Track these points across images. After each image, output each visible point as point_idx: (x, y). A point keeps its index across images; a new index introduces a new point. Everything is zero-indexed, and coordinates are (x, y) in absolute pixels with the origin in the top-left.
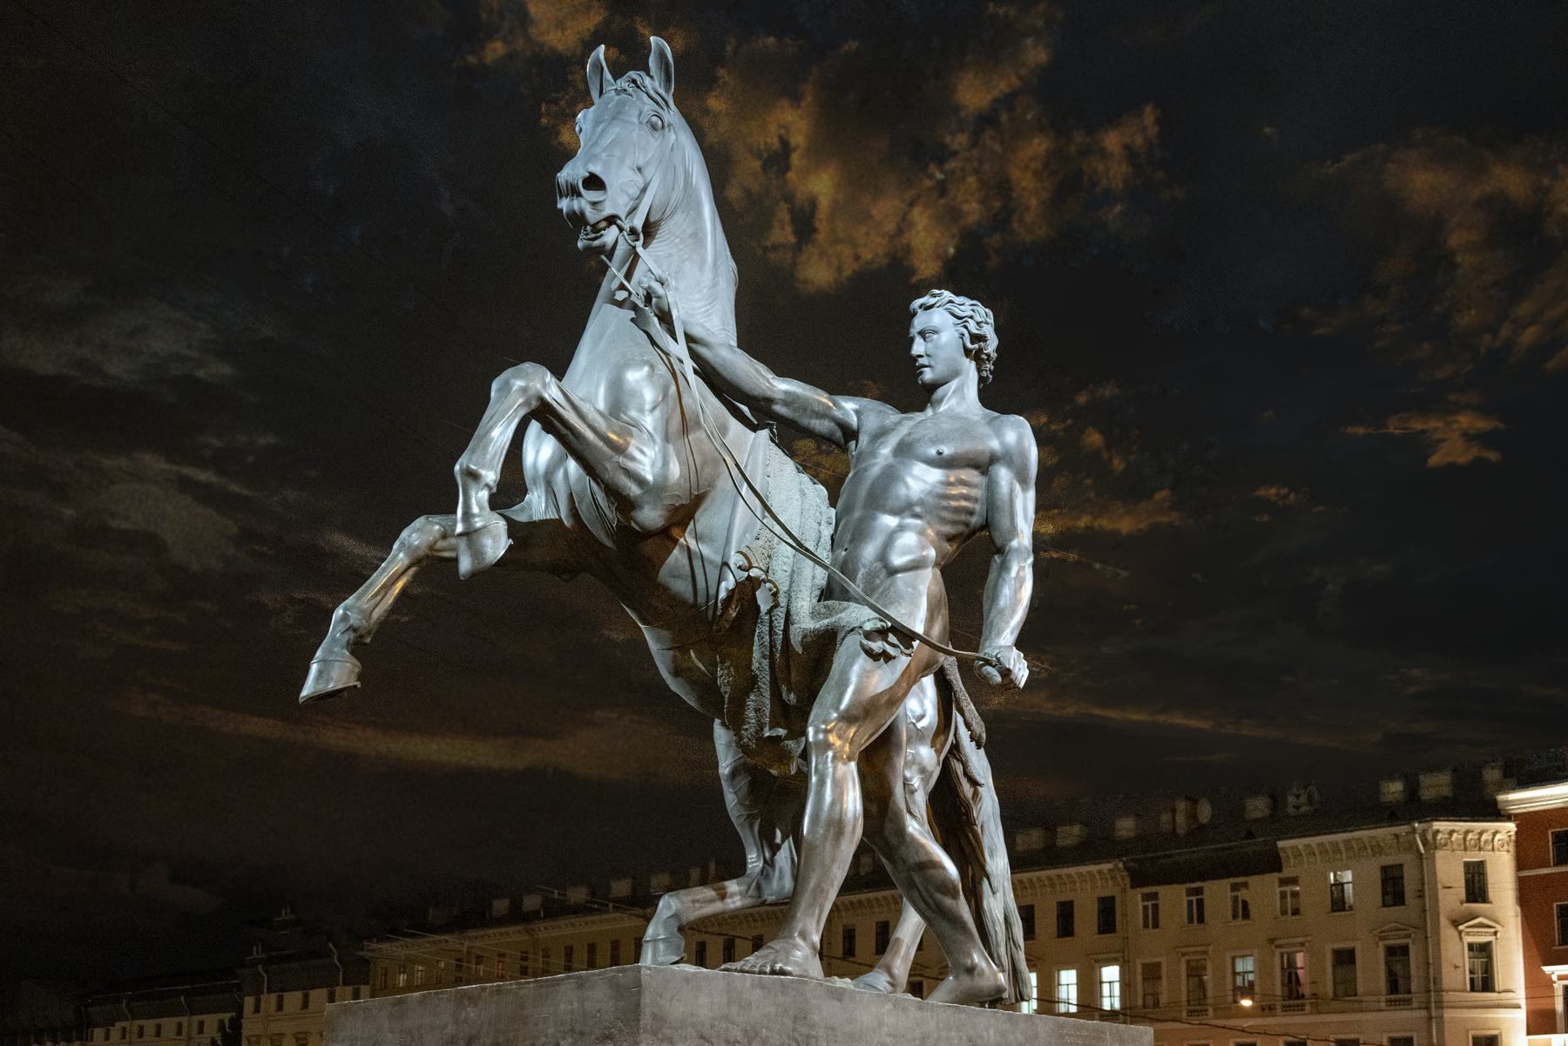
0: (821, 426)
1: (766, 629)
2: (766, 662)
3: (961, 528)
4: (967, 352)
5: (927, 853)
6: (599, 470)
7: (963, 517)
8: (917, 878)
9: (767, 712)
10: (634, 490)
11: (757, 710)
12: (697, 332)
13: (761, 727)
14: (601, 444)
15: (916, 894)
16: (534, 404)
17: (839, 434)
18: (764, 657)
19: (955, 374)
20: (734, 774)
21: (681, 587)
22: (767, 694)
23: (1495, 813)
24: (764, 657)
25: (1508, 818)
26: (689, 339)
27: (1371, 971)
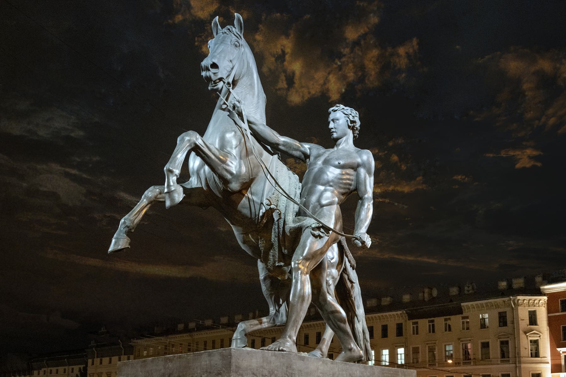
0: (296, 153)
1: (277, 227)
2: (276, 239)
3: (347, 190)
4: (349, 127)
5: (335, 307)
6: (216, 169)
7: (348, 186)
8: (331, 316)
9: (277, 257)
10: (229, 177)
11: (273, 256)
12: (252, 120)
13: (275, 262)
14: (217, 160)
15: (331, 322)
16: (193, 145)
17: (303, 156)
18: (276, 237)
19: (345, 135)
20: (265, 279)
21: (246, 212)
22: (277, 250)
23: (540, 293)
24: (276, 237)
25: (544, 295)
26: (249, 122)
27: (495, 350)
